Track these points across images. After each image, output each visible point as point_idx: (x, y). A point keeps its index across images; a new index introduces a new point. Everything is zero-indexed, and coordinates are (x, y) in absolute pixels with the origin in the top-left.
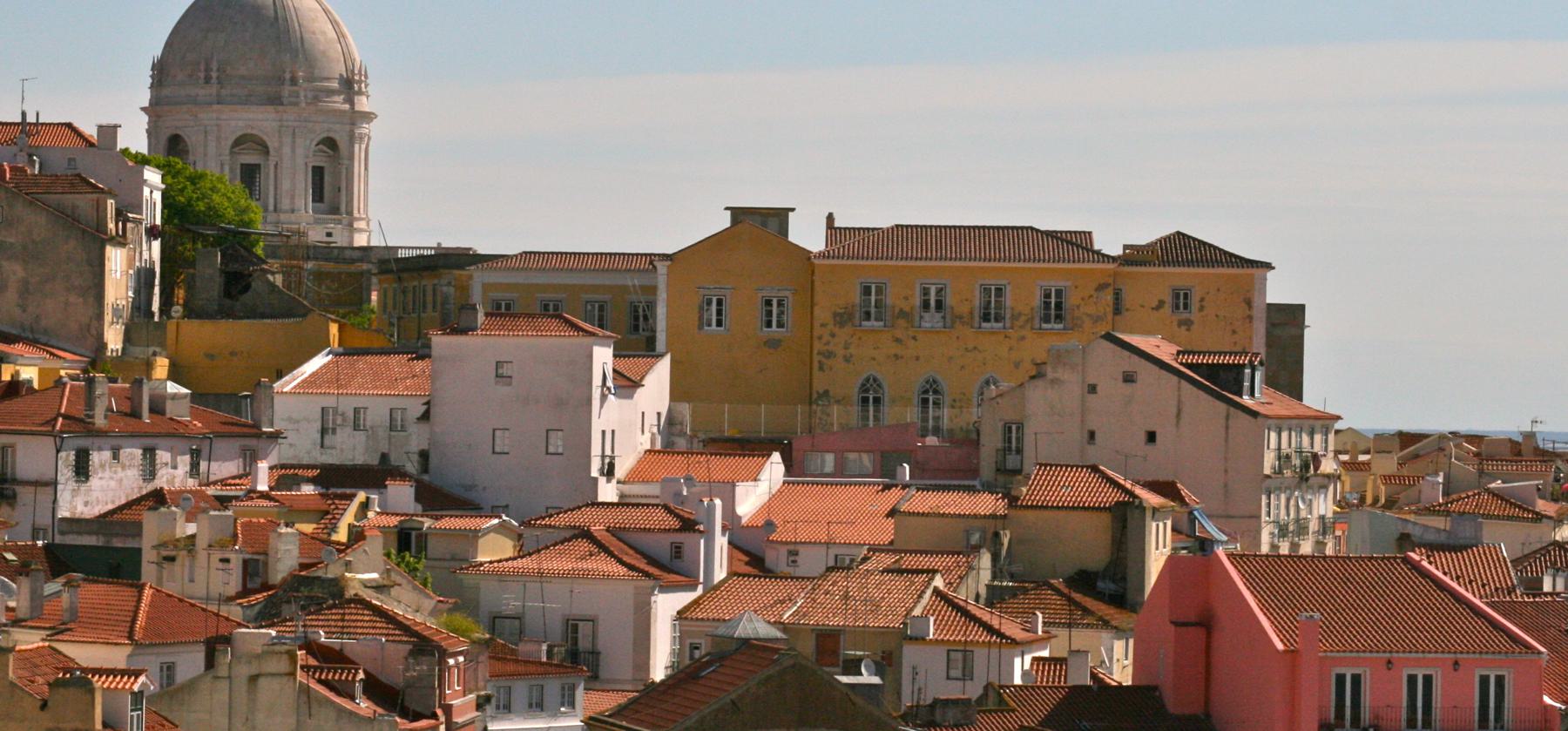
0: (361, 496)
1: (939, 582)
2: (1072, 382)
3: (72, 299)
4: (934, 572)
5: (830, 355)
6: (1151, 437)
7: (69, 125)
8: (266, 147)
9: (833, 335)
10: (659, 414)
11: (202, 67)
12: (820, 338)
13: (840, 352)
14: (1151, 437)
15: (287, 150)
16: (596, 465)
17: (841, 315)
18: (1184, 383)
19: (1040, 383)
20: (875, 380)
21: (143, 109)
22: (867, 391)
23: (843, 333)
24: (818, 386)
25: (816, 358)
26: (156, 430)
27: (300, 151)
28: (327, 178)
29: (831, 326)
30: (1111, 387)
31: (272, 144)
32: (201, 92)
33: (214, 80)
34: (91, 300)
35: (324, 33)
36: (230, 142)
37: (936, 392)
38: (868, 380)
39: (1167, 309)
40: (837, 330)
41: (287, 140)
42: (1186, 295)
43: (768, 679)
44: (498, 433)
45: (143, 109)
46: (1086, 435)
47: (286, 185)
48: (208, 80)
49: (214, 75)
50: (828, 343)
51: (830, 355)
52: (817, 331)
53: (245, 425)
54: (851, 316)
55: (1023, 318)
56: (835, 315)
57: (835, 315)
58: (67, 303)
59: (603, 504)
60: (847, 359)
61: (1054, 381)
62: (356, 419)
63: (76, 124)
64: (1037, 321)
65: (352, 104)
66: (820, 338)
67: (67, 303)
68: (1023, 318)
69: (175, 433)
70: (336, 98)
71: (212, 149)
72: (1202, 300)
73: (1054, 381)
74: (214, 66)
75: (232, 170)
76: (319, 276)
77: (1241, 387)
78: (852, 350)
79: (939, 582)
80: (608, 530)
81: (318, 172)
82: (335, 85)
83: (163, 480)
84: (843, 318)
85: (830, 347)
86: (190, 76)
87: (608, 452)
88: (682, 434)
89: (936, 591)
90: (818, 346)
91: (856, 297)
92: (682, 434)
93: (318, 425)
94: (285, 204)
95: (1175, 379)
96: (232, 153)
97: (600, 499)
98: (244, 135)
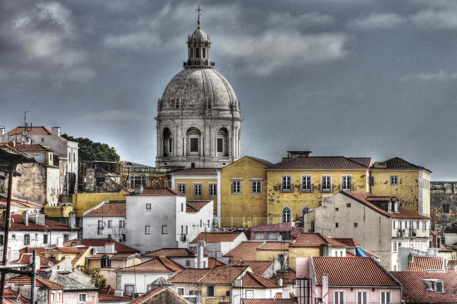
0: (91, 248)
1: (249, 269)
2: (331, 207)
3: (36, 187)
4: (248, 266)
5: (272, 200)
6: (356, 225)
7: (43, 127)
8: (199, 131)
9: (273, 194)
10: (209, 221)
11: (176, 101)
12: (269, 195)
13: (276, 199)
14: (356, 225)
15: (207, 133)
16: (178, 238)
17: (276, 187)
18: (366, 207)
19: (320, 208)
20: (288, 209)
21: (155, 118)
22: (285, 212)
23: (277, 193)
24: (269, 211)
25: (268, 202)
26: (30, 228)
27: (213, 133)
28: (224, 143)
29: (273, 191)
30: (344, 209)
31: (202, 130)
32: (175, 111)
33: (180, 107)
34: (42, 187)
35: (221, 89)
36: (186, 130)
37: (288, 212)
38: (285, 209)
39: (389, 183)
40: (275, 192)
41: (208, 129)
42: (395, 179)
43: (156, 296)
44: (147, 227)
45: (155, 118)
46: (335, 225)
47: (207, 146)
48: (178, 106)
49: (180, 104)
50: (272, 197)
51: (272, 200)
52: (268, 192)
53: (64, 226)
54: (280, 187)
55: (337, 187)
56: (274, 187)
57: (274, 187)
58: (34, 189)
59: (180, 249)
60: (278, 202)
61: (325, 207)
62: (109, 224)
63: (45, 127)
64: (341, 188)
65: (233, 115)
66: (269, 195)
67: (34, 189)
68: (337, 187)
69: (39, 229)
70: (226, 112)
71: (179, 132)
72: (401, 180)
73: (325, 207)
74: (180, 101)
75: (187, 141)
76: (151, 178)
77: (388, 209)
78: (280, 199)
79: (249, 269)
80: (167, 257)
81: (220, 141)
82: (227, 108)
83: (32, 245)
84: (276, 188)
85: (273, 198)
86: (171, 106)
87: (184, 233)
88: (218, 227)
89: (248, 273)
90: (269, 198)
91: (281, 182)
92: (218, 227)
93: (97, 226)
94: (207, 153)
95: (363, 206)
96: (187, 134)
97: (179, 247)
98: (192, 127)
